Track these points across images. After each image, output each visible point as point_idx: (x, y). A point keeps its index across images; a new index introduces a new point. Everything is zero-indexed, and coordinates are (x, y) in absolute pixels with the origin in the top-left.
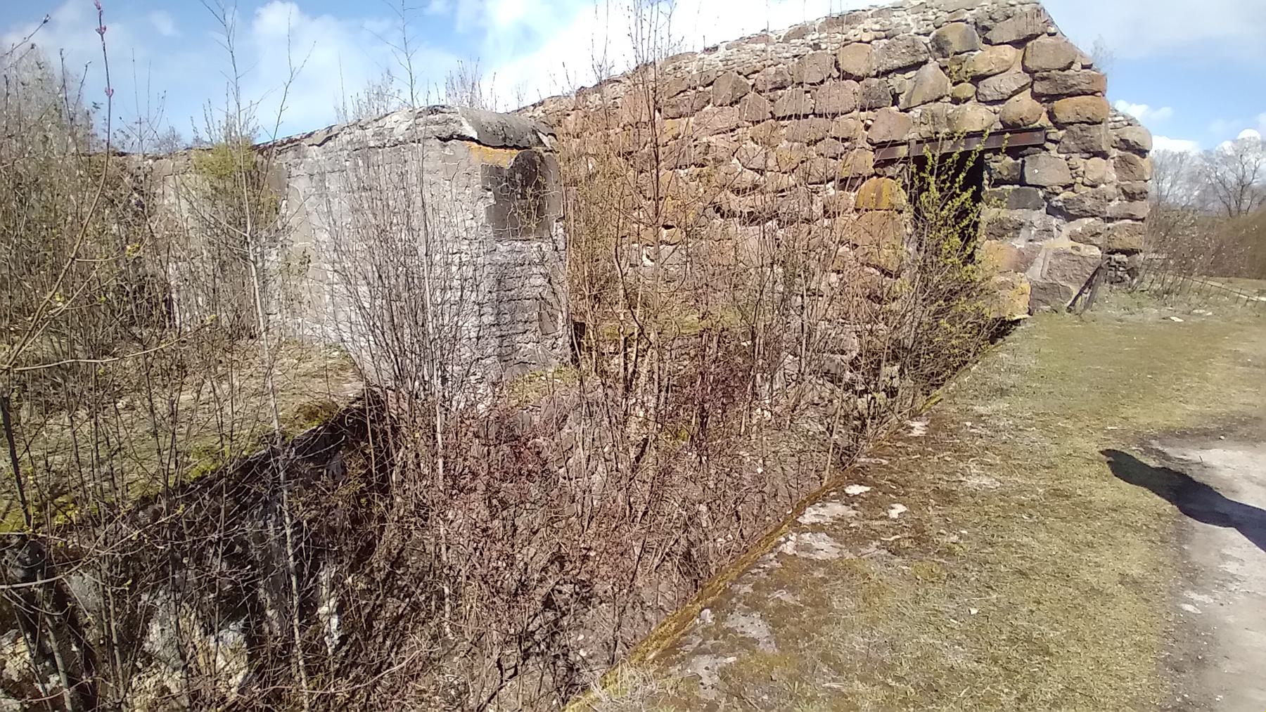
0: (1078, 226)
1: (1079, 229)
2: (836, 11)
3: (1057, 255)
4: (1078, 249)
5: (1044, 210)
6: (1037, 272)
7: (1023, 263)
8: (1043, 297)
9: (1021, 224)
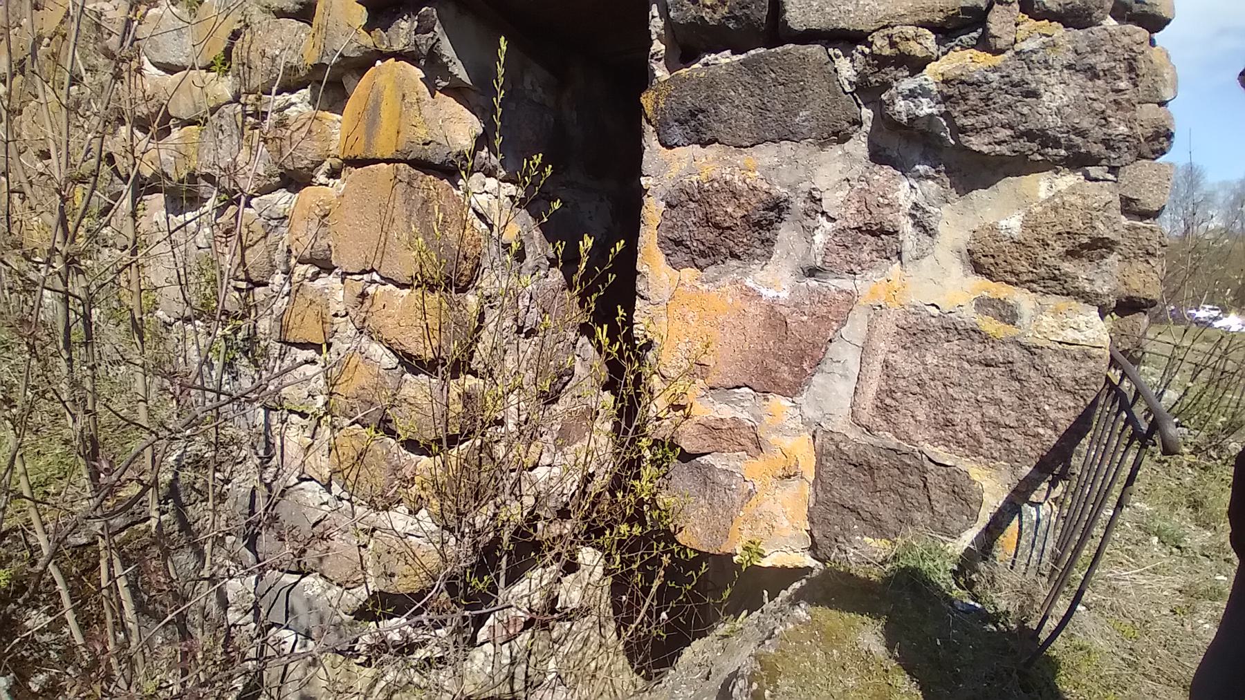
0: (1006, 209)
1: (1013, 224)
2: (1179, 84)
3: (915, 334)
4: (1009, 315)
5: (858, 146)
6: (837, 394)
7: (788, 359)
8: (865, 502)
9: (778, 207)
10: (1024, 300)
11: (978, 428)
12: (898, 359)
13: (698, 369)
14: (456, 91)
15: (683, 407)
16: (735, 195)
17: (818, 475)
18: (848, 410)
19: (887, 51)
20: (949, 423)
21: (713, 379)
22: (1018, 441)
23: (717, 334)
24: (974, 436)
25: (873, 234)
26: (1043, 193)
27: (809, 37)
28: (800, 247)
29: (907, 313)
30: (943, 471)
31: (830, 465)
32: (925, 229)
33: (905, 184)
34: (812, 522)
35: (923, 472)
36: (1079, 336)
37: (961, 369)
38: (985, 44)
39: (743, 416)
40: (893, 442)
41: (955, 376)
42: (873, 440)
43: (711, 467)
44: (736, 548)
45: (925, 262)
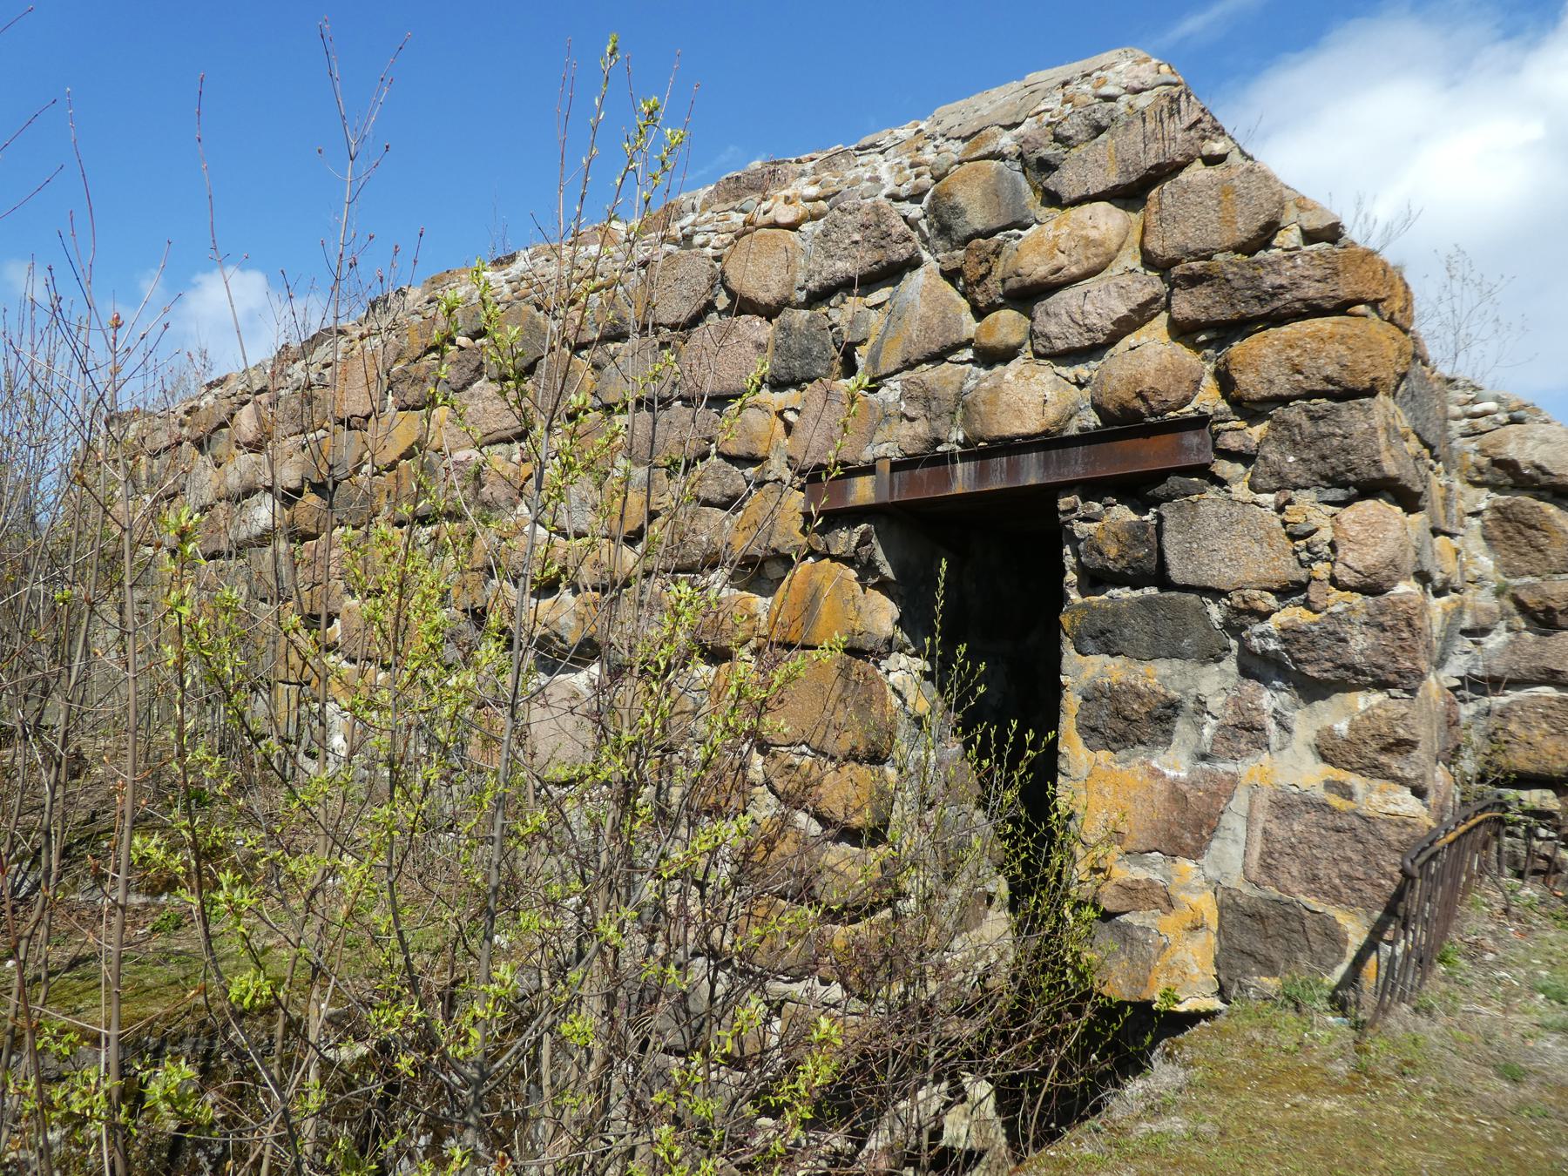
3: (1284, 807)
4: (1347, 792)
5: (1230, 665)
7: (1188, 828)
8: (1260, 947)
9: (1174, 707)
10: (1357, 782)
11: (1337, 881)
12: (1273, 827)
13: (1117, 836)
14: (883, 586)
15: (1104, 871)
16: (1139, 695)
17: (1220, 926)
18: (1240, 869)
19: (1242, 606)
20: (1315, 878)
21: (1129, 845)
22: (1369, 891)
23: (1130, 806)
24: (1335, 887)
25: (1247, 730)
26: (1361, 707)
27: (1187, 588)
28: (1193, 737)
29: (1276, 791)
30: (1316, 917)
31: (1229, 917)
32: (1284, 727)
33: (1267, 694)
34: (1218, 968)
35: (1301, 919)
36: (1399, 810)
37: (1319, 834)
38: (1307, 604)
39: (1156, 877)
40: (1276, 894)
41: (1317, 839)
42: (1262, 894)
43: (1129, 925)
44: (1156, 996)
45: (1286, 752)
